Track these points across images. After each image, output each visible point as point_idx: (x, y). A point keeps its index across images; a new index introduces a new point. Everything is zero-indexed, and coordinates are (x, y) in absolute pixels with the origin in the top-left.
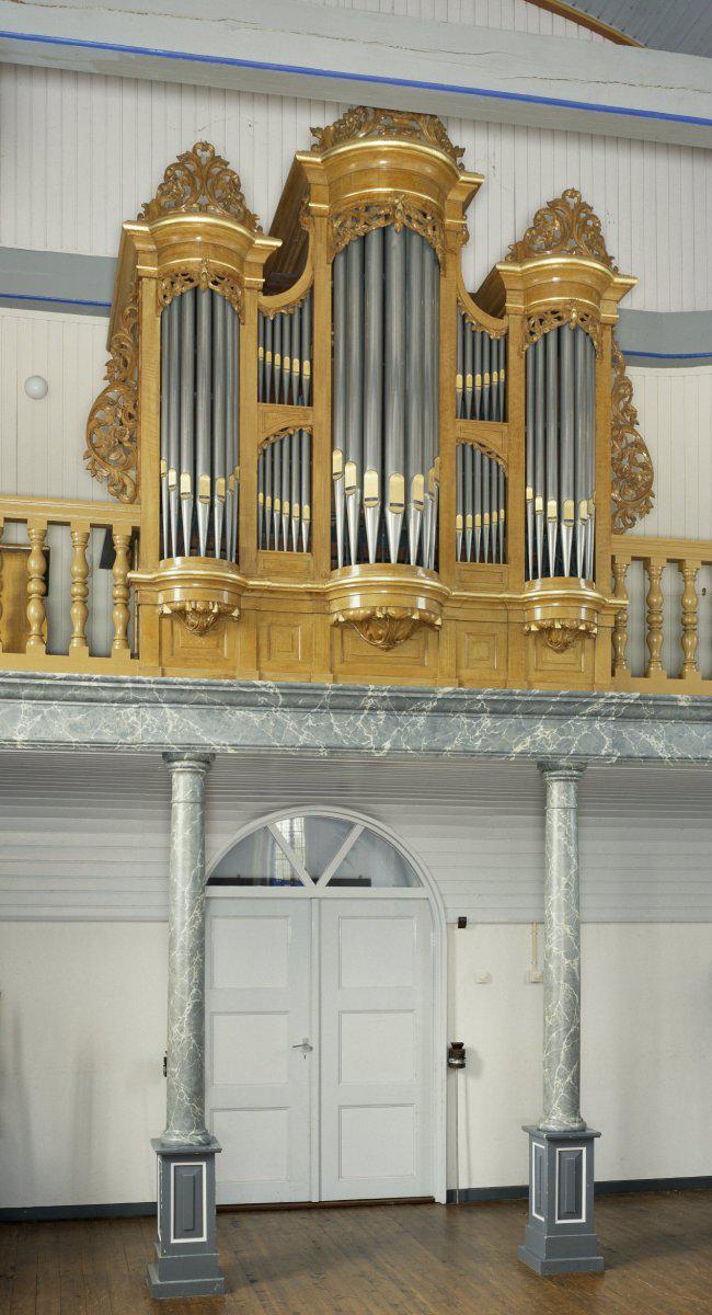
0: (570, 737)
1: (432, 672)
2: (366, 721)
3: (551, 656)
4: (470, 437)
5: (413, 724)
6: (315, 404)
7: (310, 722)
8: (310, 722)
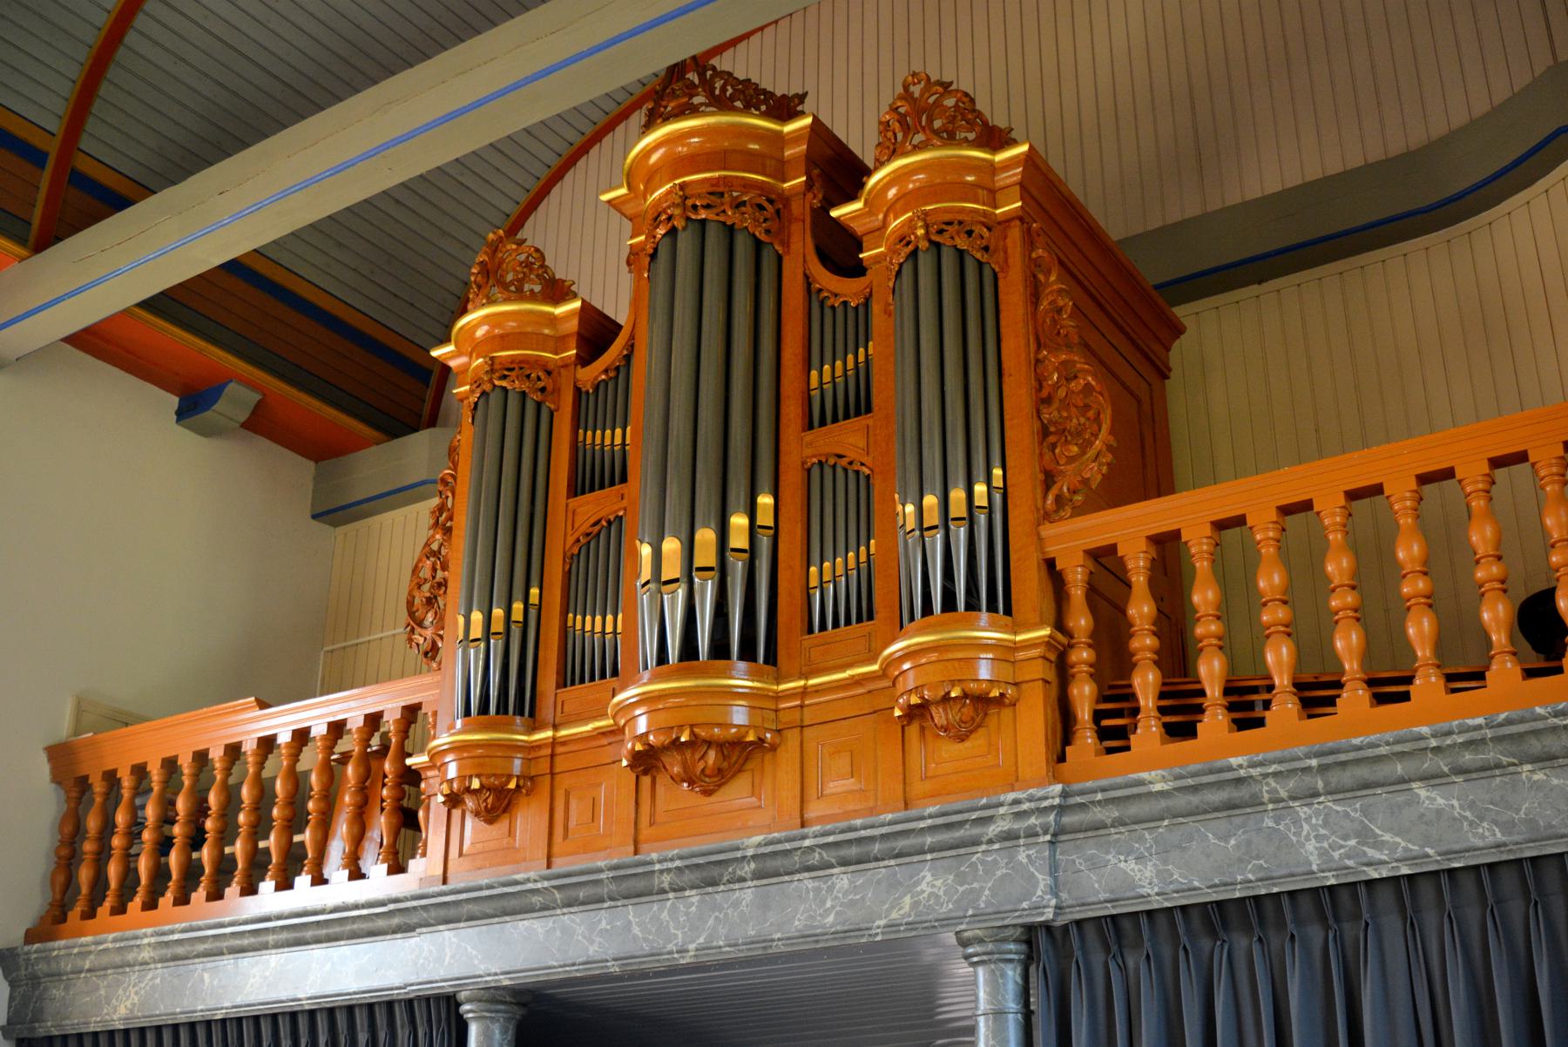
0: (975, 885)
1: (749, 815)
2: (673, 911)
3: (949, 750)
4: (827, 450)
5: (736, 904)
6: (629, 478)
7: (604, 925)
8: (604, 925)
